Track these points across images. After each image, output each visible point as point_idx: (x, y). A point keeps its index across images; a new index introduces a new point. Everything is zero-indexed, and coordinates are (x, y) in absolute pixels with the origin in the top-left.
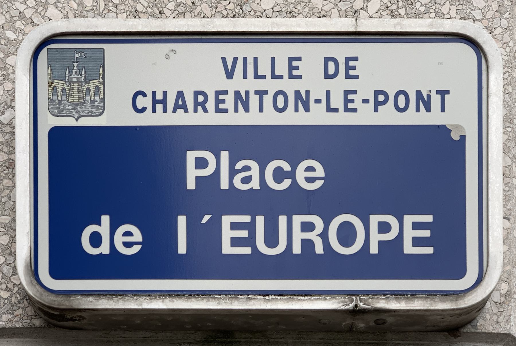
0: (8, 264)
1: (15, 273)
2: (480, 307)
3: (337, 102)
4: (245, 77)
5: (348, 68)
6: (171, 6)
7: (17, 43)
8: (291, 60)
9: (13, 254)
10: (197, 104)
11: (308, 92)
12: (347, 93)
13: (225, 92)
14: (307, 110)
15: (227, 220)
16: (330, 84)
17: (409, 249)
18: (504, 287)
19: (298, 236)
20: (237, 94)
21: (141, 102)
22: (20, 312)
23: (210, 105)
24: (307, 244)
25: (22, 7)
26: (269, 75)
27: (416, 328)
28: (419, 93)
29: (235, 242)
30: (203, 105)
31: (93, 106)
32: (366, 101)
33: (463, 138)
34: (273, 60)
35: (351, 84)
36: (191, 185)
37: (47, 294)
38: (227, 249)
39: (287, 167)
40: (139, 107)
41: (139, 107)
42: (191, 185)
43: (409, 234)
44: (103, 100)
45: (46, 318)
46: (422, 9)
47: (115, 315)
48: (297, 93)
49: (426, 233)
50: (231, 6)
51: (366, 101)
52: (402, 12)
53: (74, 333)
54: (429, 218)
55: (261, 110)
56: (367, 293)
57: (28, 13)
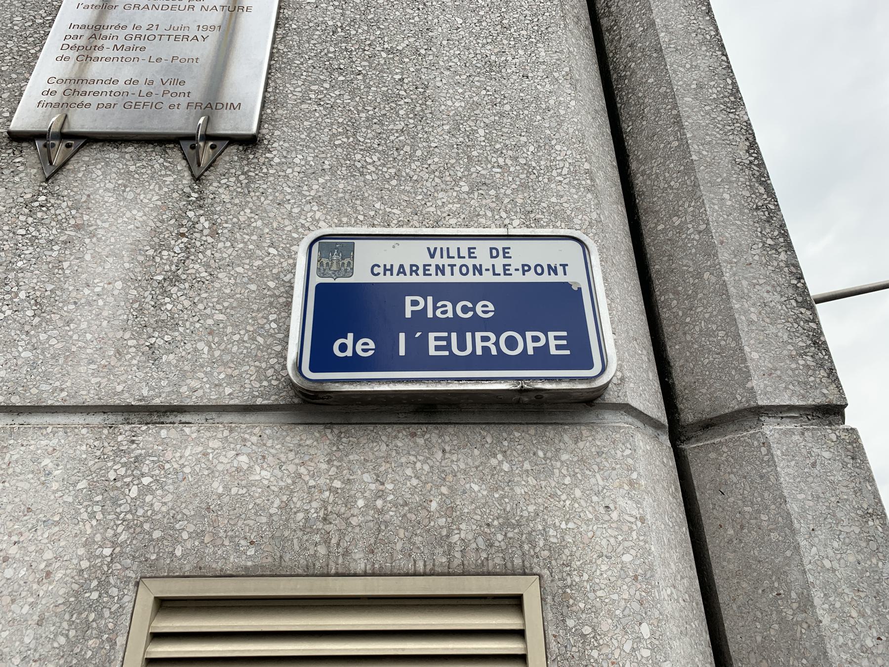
0: (279, 364)
1: (284, 367)
2: (605, 387)
3: (499, 269)
4: (442, 257)
5: (504, 253)
6: (395, 222)
7: (300, 239)
8: (469, 249)
9: (285, 359)
10: (411, 271)
11: (481, 265)
12: (504, 266)
13: (430, 265)
14: (481, 274)
15: (432, 336)
16: (494, 261)
17: (553, 351)
18: (619, 374)
19: (479, 344)
20: (437, 266)
21: (376, 270)
22: (284, 394)
23: (421, 272)
24: (486, 349)
25: (303, 222)
26: (456, 256)
27: (563, 401)
28: (549, 266)
29: (437, 348)
30: (416, 272)
31: (346, 272)
32: (517, 270)
33: (580, 289)
34: (459, 249)
35: (507, 261)
36: (408, 315)
37: (306, 381)
38: (432, 352)
39: (470, 305)
40: (375, 272)
41: (375, 272)
42: (408, 315)
43: (553, 343)
44: (352, 269)
45: (304, 397)
46: (545, 224)
47: (354, 395)
48: (474, 266)
49: (564, 342)
50: (431, 222)
51: (517, 270)
52: (533, 225)
53: (322, 407)
54: (565, 334)
55: (452, 274)
56: (529, 379)
57: (307, 225)
